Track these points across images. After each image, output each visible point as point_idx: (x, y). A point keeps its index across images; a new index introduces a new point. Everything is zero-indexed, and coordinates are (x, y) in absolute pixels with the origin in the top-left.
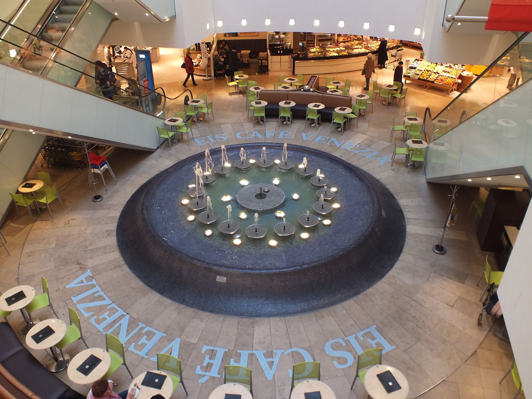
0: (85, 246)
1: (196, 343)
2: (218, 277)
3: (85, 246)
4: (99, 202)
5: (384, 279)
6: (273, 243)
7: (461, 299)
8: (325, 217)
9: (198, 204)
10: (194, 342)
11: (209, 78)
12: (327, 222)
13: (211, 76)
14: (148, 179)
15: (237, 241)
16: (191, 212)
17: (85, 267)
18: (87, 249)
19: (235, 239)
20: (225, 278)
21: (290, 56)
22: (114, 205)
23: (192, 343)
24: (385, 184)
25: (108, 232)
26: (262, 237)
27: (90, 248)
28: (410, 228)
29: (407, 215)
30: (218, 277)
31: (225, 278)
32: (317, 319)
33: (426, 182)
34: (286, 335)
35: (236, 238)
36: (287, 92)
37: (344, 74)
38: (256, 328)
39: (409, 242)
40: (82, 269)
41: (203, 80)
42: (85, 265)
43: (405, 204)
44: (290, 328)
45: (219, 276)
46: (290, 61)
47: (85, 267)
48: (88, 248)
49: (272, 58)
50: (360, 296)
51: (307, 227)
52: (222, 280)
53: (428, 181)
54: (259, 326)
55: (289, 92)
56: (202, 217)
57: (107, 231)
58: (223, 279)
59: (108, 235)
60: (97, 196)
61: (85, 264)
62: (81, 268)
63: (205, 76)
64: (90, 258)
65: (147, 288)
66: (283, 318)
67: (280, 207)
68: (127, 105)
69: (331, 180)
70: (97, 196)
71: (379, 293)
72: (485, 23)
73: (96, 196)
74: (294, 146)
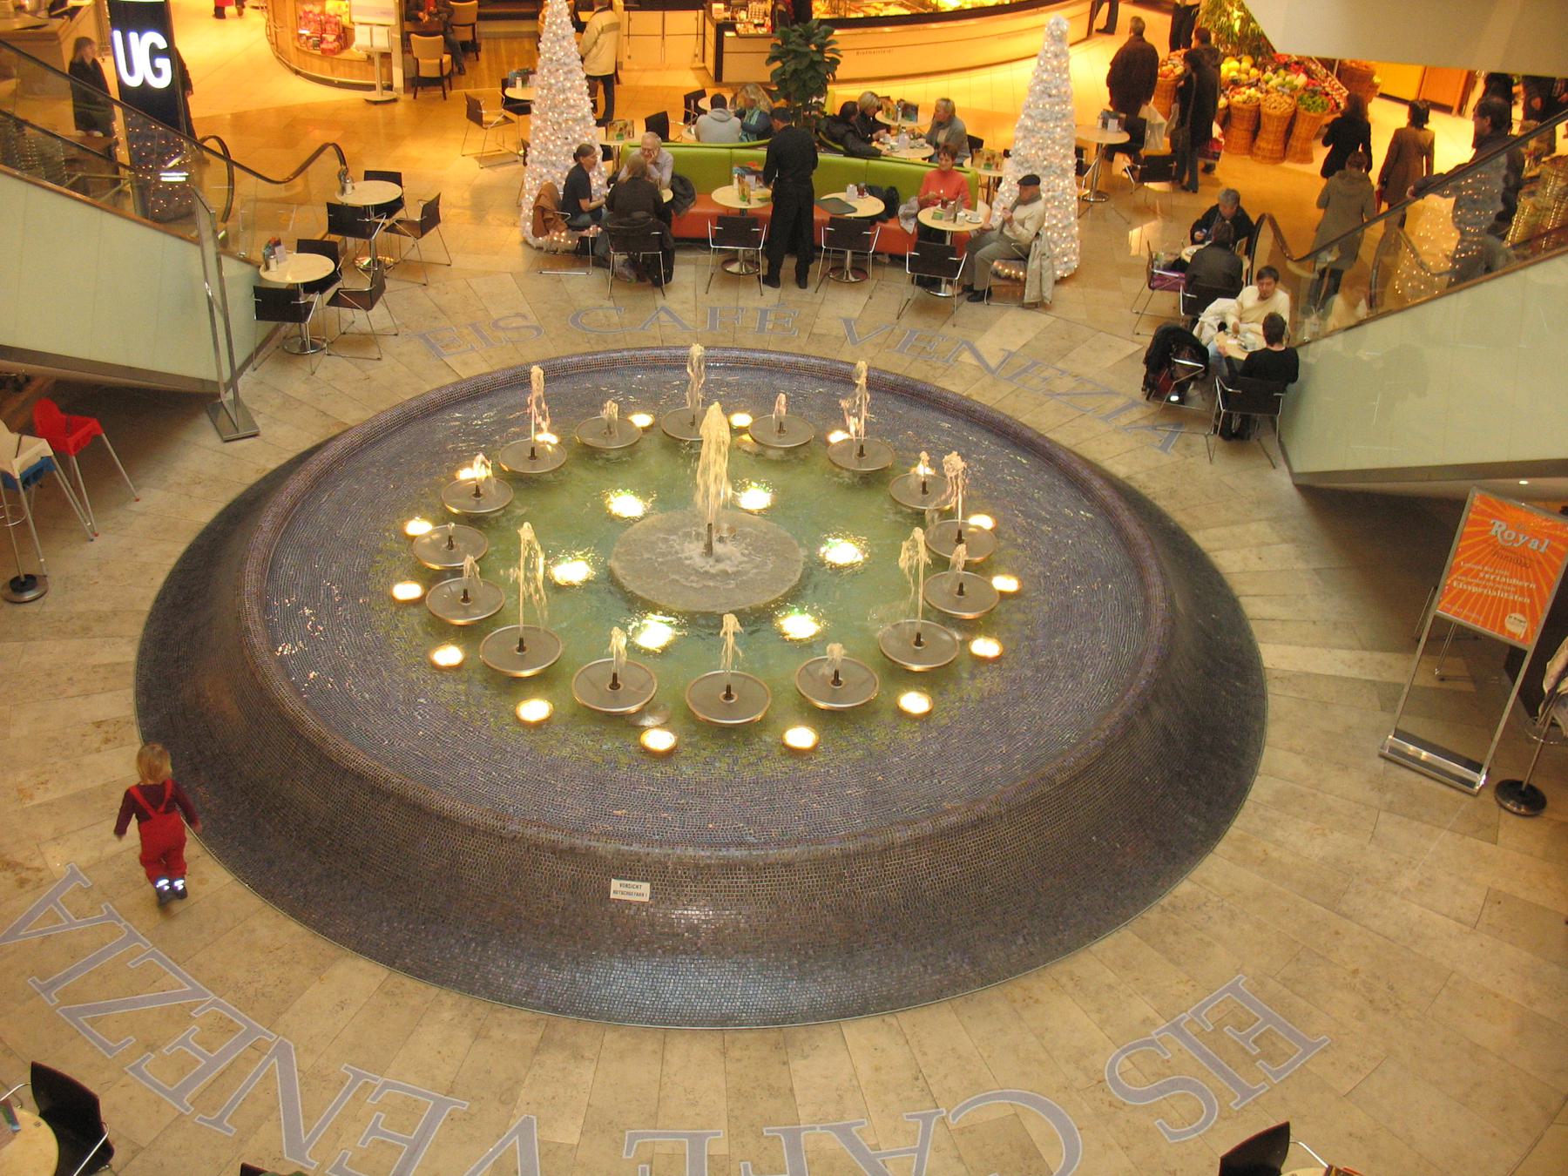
0: (20, 791)
1: (576, 1143)
2: (615, 884)
3: (20, 791)
4: (33, 609)
5: (1221, 847)
6: (801, 737)
7: (1495, 898)
8: (972, 628)
9: (836, 681)
10: (569, 1141)
11: (388, 95)
12: (985, 647)
13: (390, 88)
14: (221, 506)
15: (659, 739)
16: (443, 632)
17: (41, 875)
18: (29, 804)
19: (643, 729)
20: (645, 888)
21: (701, 12)
22: (101, 618)
23: (560, 1146)
24: (1150, 497)
25: (104, 728)
26: (759, 716)
27: (41, 797)
28: (1273, 655)
29: (1254, 607)
30: (615, 884)
31: (645, 888)
32: (1015, 1010)
33: (1292, 486)
34: (917, 1079)
35: (650, 728)
36: (727, 151)
37: (908, 81)
38: (798, 1065)
39: (1279, 702)
40: (28, 887)
41: (367, 101)
42: (38, 870)
43: (1236, 568)
44: (925, 1054)
45: (621, 878)
46: (701, 31)
47: (41, 875)
48: (31, 797)
49: (630, 20)
50: (1152, 915)
51: (916, 668)
52: (629, 894)
53: (1299, 482)
54: (805, 1057)
55: (734, 150)
56: (491, 651)
57: (99, 724)
58: (638, 891)
59: (107, 741)
60: (23, 579)
61: (37, 863)
62: (22, 883)
63: (371, 88)
64: (54, 839)
65: (322, 945)
66: (890, 1019)
67: (794, 597)
68: (98, 202)
69: (982, 494)
70: (23, 579)
71: (1216, 899)
72: (369, 44)
73: (17, 578)
74: (794, 359)
